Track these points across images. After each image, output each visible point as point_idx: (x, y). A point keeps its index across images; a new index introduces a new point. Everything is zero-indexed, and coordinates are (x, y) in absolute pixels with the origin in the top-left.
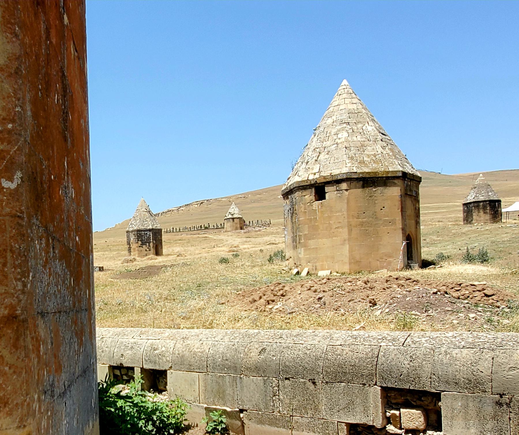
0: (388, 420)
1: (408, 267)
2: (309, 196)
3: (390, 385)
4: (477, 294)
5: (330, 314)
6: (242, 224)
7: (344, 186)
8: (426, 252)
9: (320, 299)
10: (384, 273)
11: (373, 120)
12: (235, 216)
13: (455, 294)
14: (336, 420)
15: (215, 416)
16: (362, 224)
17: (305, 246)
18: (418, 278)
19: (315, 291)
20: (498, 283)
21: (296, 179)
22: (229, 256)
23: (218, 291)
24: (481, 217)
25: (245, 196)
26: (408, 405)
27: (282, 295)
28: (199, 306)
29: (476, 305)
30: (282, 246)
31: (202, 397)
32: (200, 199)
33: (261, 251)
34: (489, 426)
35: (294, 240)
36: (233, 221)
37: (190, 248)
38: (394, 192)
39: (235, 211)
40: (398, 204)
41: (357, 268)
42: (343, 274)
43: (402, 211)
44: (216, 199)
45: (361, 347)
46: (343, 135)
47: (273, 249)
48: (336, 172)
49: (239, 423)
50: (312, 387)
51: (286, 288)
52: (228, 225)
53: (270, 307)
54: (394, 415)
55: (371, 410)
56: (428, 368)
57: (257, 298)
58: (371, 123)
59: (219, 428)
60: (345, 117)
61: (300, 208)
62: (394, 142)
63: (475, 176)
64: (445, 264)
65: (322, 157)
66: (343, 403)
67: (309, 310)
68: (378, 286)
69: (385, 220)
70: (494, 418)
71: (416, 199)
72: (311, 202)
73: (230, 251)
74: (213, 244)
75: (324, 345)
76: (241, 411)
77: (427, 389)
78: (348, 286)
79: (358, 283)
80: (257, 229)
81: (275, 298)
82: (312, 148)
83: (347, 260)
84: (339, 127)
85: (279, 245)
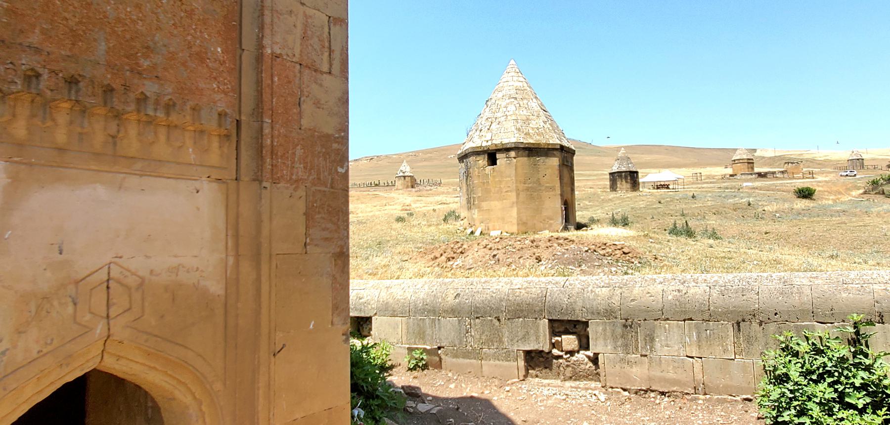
0: (553, 345)
1: (566, 228)
2: (482, 161)
3: (554, 318)
4: (617, 252)
5: (504, 269)
6: (413, 183)
7: (513, 154)
8: (580, 216)
9: (494, 256)
10: (547, 234)
11: (536, 98)
12: (406, 174)
13: (602, 252)
14: (515, 348)
15: (417, 354)
16: (527, 189)
17: (479, 207)
18: (574, 238)
19: (490, 249)
20: (634, 244)
21: (469, 145)
22: (404, 214)
23: (399, 249)
24: (623, 185)
25: (416, 154)
26: (567, 332)
27: (462, 253)
28: (383, 263)
29: (617, 261)
30: (453, 207)
31: (404, 339)
32: (371, 154)
33: (434, 210)
34: (619, 343)
35: (469, 202)
36: (492, 161)
37: (360, 206)
38: (554, 161)
39: (406, 168)
40: (557, 172)
41: (524, 229)
42: (512, 234)
43: (560, 179)
44: (386, 156)
45: (534, 290)
46: (512, 108)
47: (446, 209)
48: (505, 141)
49: (438, 359)
50: (497, 323)
51: (465, 246)
52: (399, 183)
53: (451, 263)
54: (557, 341)
55: (541, 339)
56: (580, 304)
57: (438, 256)
58: (534, 100)
59: (420, 364)
60: (513, 92)
61: (475, 172)
62: (554, 118)
63: (618, 149)
64: (594, 226)
65: (494, 126)
66: (520, 334)
67: (485, 266)
68: (542, 245)
69: (547, 187)
70: (622, 337)
71: (571, 169)
72: (484, 167)
73: (403, 210)
74: (384, 202)
75: (506, 289)
76: (439, 348)
77: (579, 319)
78: (518, 245)
79: (527, 242)
80: (429, 188)
81: (454, 255)
82: (485, 118)
83: (515, 221)
84: (508, 101)
85: (451, 205)
